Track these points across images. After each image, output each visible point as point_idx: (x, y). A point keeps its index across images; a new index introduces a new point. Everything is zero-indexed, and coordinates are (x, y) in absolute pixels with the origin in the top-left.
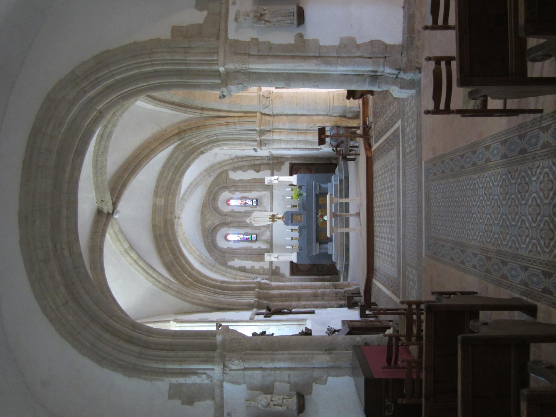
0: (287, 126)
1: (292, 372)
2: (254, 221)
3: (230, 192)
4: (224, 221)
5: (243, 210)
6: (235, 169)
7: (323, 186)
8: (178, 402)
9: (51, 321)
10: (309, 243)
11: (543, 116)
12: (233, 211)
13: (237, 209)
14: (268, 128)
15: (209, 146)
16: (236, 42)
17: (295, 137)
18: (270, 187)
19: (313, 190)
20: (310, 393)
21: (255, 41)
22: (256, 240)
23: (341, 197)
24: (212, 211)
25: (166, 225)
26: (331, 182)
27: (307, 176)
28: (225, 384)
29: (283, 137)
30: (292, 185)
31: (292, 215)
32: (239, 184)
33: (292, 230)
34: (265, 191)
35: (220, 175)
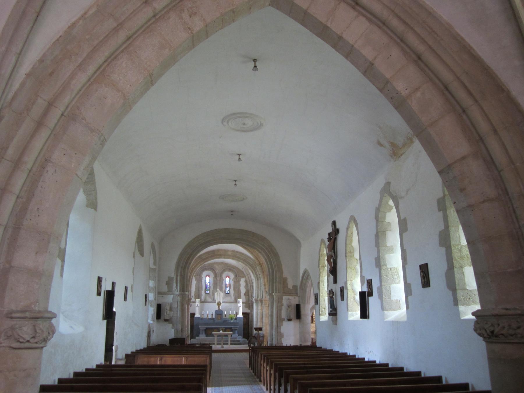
0: (264, 313)
1: (176, 317)
2: (218, 293)
3: (234, 278)
4: (218, 276)
5: (224, 286)
6: (246, 281)
7: (236, 332)
8: (167, 279)
9: (194, 239)
10: (205, 324)
11: (158, 14)
12: (223, 280)
13: (224, 282)
14: (263, 304)
15: (255, 276)
16: (282, 299)
17: (259, 317)
18: (236, 302)
19: (234, 326)
20: (169, 323)
21: (283, 305)
22: (206, 293)
23: (231, 341)
24: (223, 268)
25: (219, 255)
26: (238, 336)
27: (241, 323)
28: (172, 296)
29: (259, 311)
30: (237, 314)
31: (221, 314)
32: (238, 284)
33: (212, 314)
34: (234, 298)
35: (243, 273)
